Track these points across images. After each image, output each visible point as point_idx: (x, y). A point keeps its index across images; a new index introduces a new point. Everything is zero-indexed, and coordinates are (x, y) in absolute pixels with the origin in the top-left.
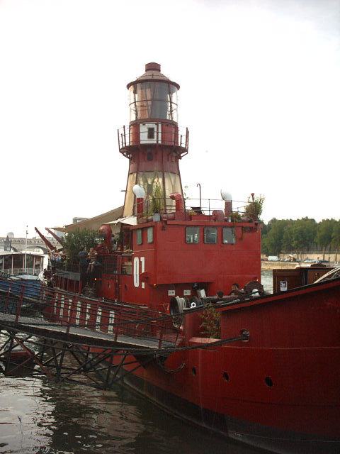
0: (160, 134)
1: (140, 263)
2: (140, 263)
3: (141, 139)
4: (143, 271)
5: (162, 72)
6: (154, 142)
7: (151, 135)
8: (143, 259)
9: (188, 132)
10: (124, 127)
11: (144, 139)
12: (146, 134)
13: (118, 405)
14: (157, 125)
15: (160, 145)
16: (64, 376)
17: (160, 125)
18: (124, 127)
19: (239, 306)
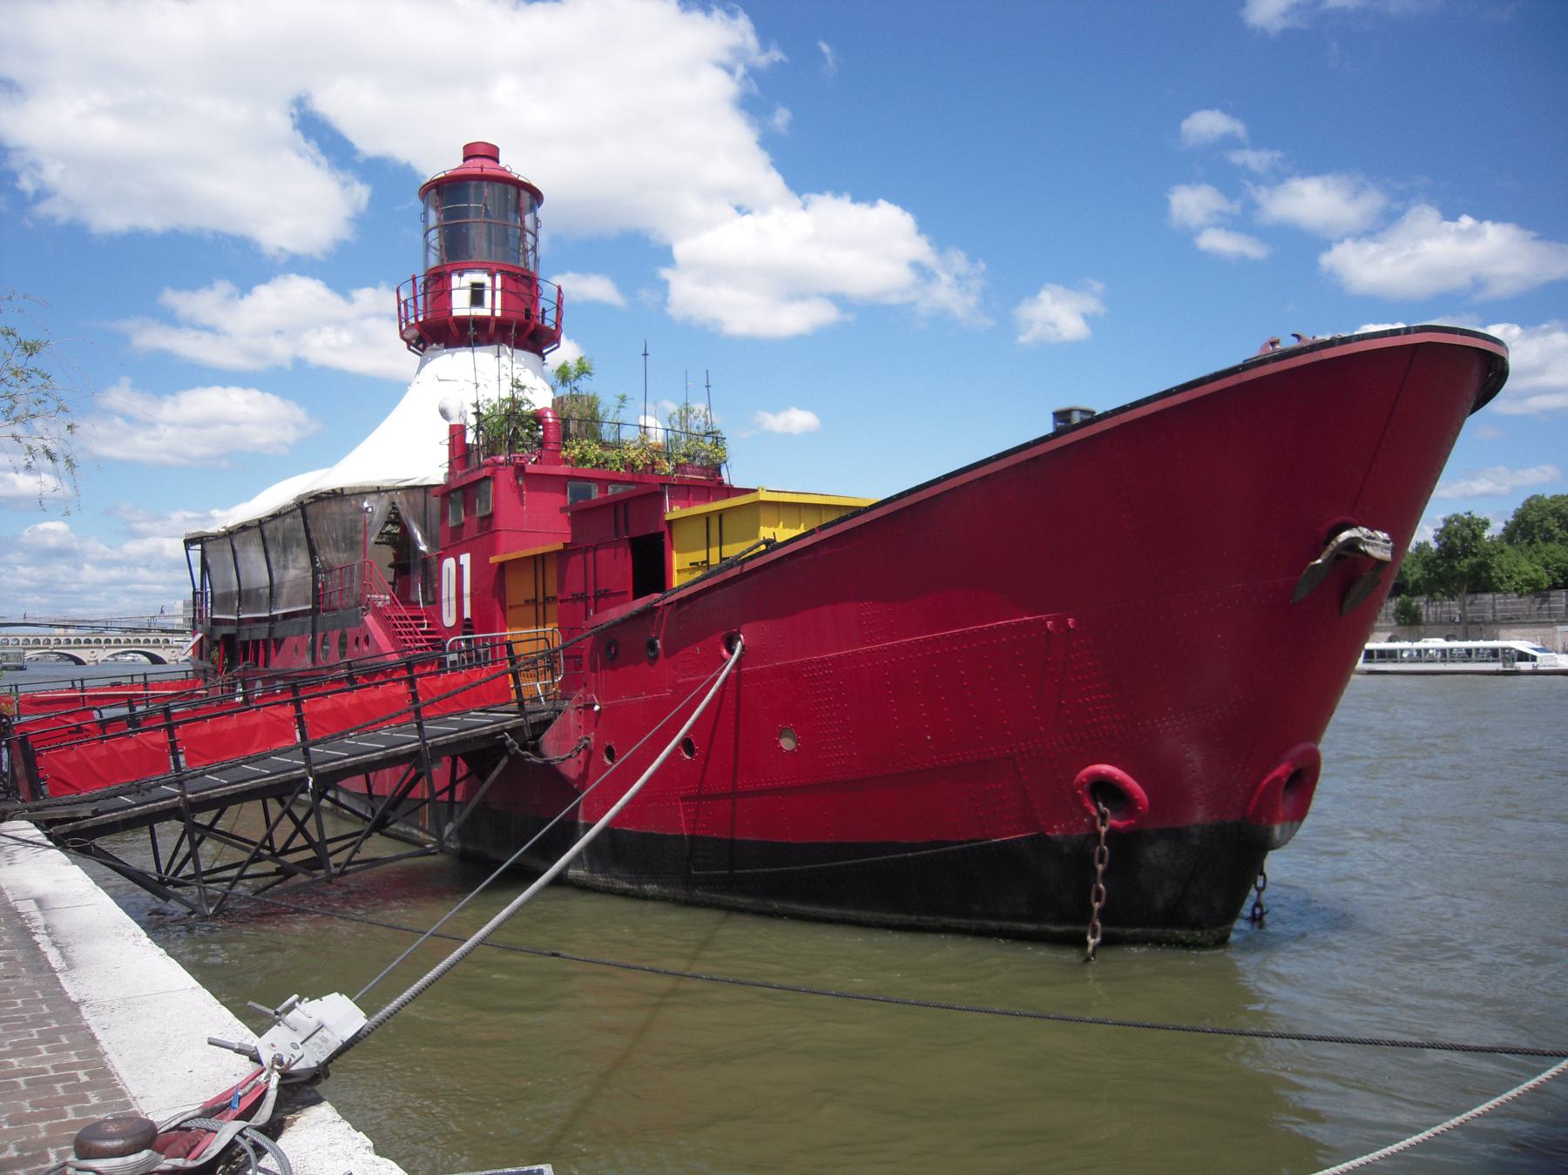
0: (498, 294)
1: (459, 568)
2: (459, 568)
3: (454, 305)
4: (467, 614)
5: (502, 164)
6: (484, 312)
7: (477, 297)
8: (465, 559)
9: (560, 300)
10: (414, 279)
11: (461, 305)
12: (467, 294)
13: (1315, 1117)
14: (493, 276)
15: (497, 319)
16: (341, 858)
17: (498, 278)
18: (414, 279)
19: (704, 585)
